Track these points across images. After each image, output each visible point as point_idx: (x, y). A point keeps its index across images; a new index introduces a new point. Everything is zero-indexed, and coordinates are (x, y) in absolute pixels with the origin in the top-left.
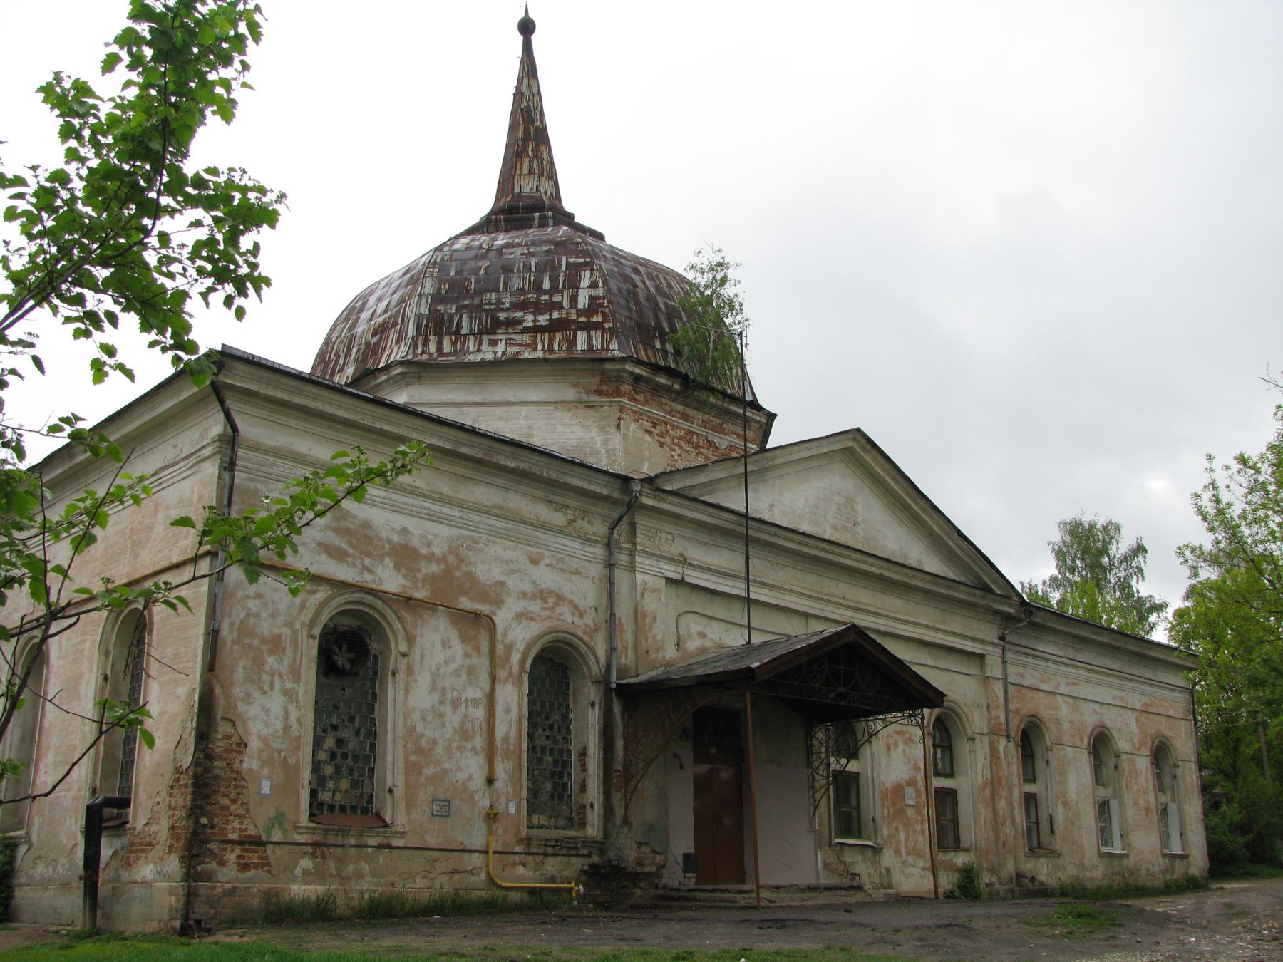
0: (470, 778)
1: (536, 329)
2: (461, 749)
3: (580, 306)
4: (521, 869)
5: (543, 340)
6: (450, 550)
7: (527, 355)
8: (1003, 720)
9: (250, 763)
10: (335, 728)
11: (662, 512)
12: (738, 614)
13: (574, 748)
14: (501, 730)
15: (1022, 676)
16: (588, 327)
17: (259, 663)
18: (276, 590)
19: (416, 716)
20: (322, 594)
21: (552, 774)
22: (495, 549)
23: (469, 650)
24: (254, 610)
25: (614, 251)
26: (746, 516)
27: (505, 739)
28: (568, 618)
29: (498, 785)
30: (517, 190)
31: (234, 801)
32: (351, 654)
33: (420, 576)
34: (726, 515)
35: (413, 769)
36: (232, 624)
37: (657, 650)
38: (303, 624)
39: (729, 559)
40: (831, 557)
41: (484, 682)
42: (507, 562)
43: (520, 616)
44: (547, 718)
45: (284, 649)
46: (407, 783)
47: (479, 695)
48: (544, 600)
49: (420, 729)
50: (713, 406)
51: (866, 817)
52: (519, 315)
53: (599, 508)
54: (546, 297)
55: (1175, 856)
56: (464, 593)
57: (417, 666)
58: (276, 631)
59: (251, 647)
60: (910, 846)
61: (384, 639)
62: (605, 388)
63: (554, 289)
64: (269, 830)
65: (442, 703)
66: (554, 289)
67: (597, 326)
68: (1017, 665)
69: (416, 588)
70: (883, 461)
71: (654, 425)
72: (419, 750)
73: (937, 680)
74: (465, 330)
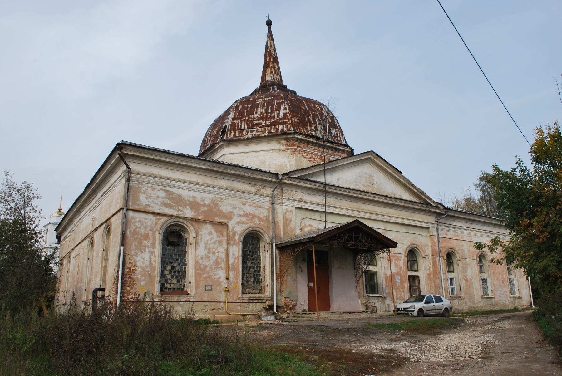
0: (220, 277)
1: (266, 126)
2: (216, 268)
3: (280, 117)
4: (239, 308)
5: (268, 129)
6: (212, 202)
7: (263, 135)
8: (437, 250)
9: (137, 276)
10: (171, 263)
14: (231, 261)
15: (447, 235)
16: (283, 123)
17: (140, 242)
18: (146, 219)
19: (199, 258)
20: (163, 219)
21: (254, 275)
22: (230, 201)
23: (219, 235)
24: (138, 226)
27: (233, 264)
28: (257, 222)
29: (231, 279)
30: (267, 79)
31: (132, 288)
32: (174, 238)
33: (200, 211)
34: (317, 184)
35: (196, 275)
36: (130, 231)
37: (292, 232)
38: (156, 230)
39: (319, 199)
40: (361, 196)
42: (233, 205)
43: (238, 223)
44: (252, 256)
45: (149, 239)
47: (223, 250)
48: (248, 217)
49: (201, 262)
50: (329, 147)
51: (380, 287)
52: (260, 121)
54: (269, 115)
55: (516, 298)
56: (217, 216)
57: (199, 241)
58: (147, 232)
59: (137, 238)
60: (399, 295)
62: (289, 144)
65: (209, 253)
67: (286, 123)
68: (444, 230)
69: (199, 216)
70: (383, 161)
71: (307, 155)
72: (200, 269)
73: (391, 236)
74: (243, 128)
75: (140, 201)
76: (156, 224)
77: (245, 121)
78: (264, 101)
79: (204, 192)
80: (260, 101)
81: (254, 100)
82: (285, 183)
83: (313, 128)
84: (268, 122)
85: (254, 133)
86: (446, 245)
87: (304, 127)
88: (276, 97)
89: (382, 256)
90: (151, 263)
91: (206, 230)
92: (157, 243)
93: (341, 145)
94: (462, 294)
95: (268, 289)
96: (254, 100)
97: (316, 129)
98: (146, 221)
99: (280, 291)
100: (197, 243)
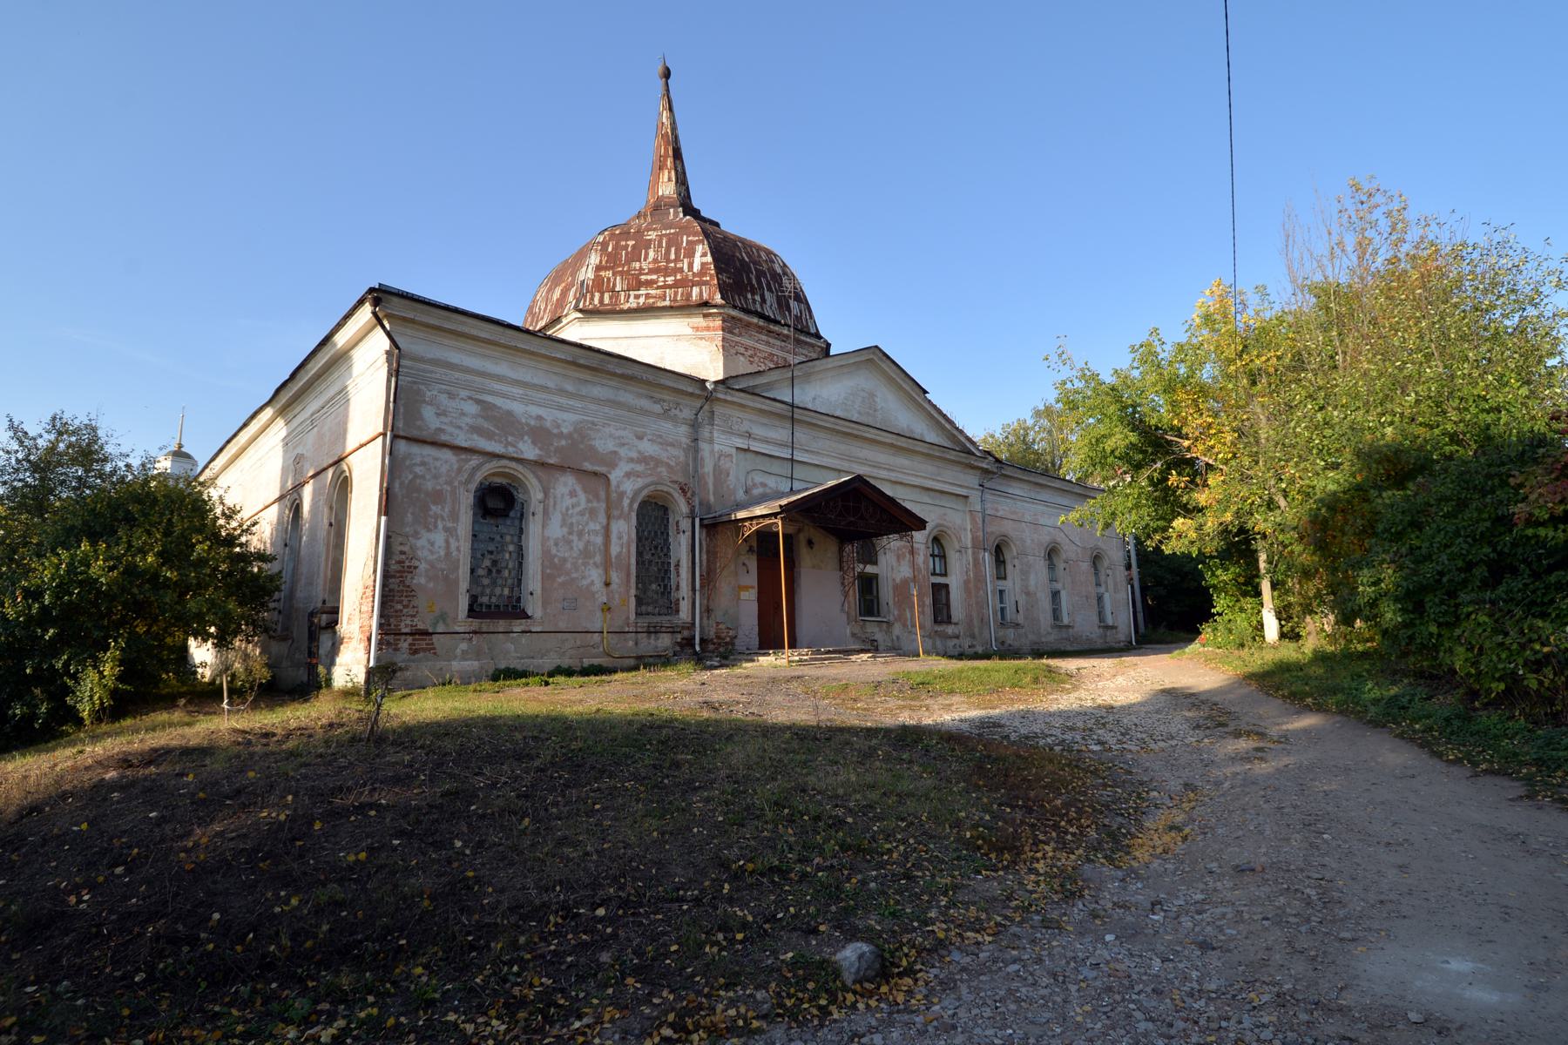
0: (592, 583)
1: (665, 287)
2: (585, 564)
9: (419, 580)
11: (733, 403)
12: (785, 469)
13: (673, 562)
16: (701, 284)
20: (475, 461)
25: (723, 232)
26: (792, 406)
27: (619, 555)
29: (614, 586)
35: (546, 578)
36: (402, 484)
39: (782, 434)
41: (602, 519)
46: (543, 589)
47: (598, 527)
49: (554, 551)
53: (686, 401)
61: (526, 491)
63: (677, 260)
64: (435, 625)
66: (677, 260)
67: (705, 283)
75: (422, 419)
76: (460, 470)
77: (621, 273)
78: (661, 237)
79: (561, 408)
80: (652, 235)
81: (639, 232)
82: (718, 399)
83: (758, 298)
84: (670, 280)
85: (642, 300)
86: (995, 528)
87: (742, 294)
88: (684, 229)
89: (891, 545)
90: (448, 554)
91: (565, 485)
92: (463, 510)
93: (809, 334)
94: (1020, 619)
95: (685, 607)
96: (639, 232)
97: (763, 301)
98: (438, 464)
99: (708, 611)
100: (546, 512)
